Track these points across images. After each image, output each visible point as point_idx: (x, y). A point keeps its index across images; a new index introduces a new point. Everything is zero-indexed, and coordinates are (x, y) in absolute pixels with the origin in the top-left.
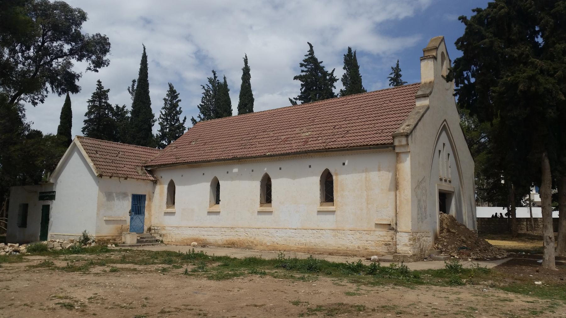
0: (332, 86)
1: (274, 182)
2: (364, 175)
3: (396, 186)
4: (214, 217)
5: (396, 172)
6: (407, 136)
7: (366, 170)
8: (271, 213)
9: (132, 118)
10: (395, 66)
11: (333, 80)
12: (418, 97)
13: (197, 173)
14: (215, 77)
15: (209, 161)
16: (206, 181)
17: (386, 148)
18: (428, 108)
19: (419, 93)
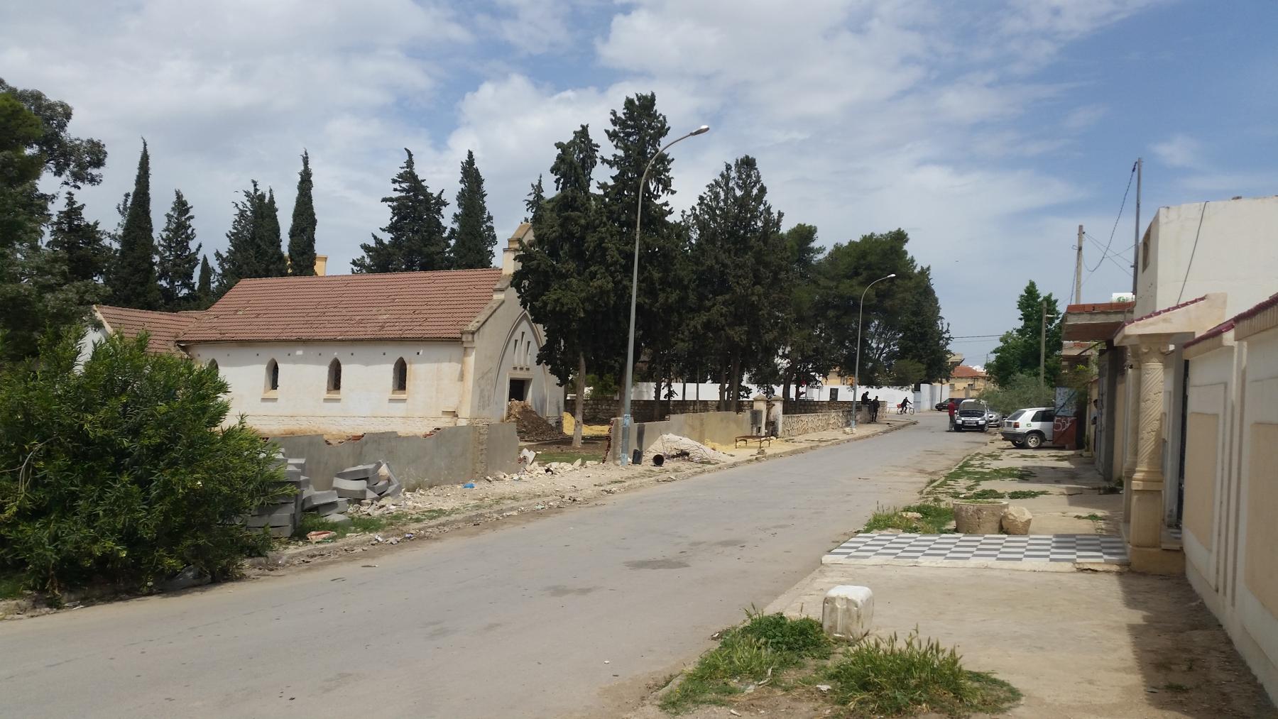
0: (439, 211)
1: (343, 367)
2: (436, 365)
3: (462, 377)
4: (269, 404)
5: (462, 362)
6: (473, 333)
7: (438, 361)
8: (339, 400)
9: (122, 253)
10: (536, 183)
11: (441, 203)
12: (495, 290)
13: (249, 352)
14: (256, 190)
15: (267, 341)
16: (261, 363)
17: (455, 342)
18: (503, 302)
19: (498, 286)
